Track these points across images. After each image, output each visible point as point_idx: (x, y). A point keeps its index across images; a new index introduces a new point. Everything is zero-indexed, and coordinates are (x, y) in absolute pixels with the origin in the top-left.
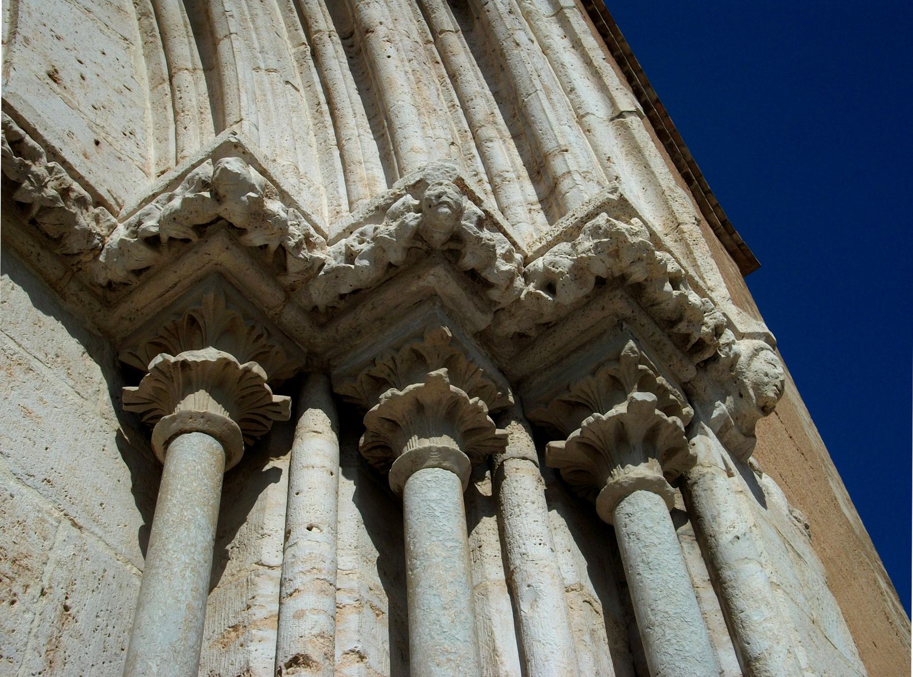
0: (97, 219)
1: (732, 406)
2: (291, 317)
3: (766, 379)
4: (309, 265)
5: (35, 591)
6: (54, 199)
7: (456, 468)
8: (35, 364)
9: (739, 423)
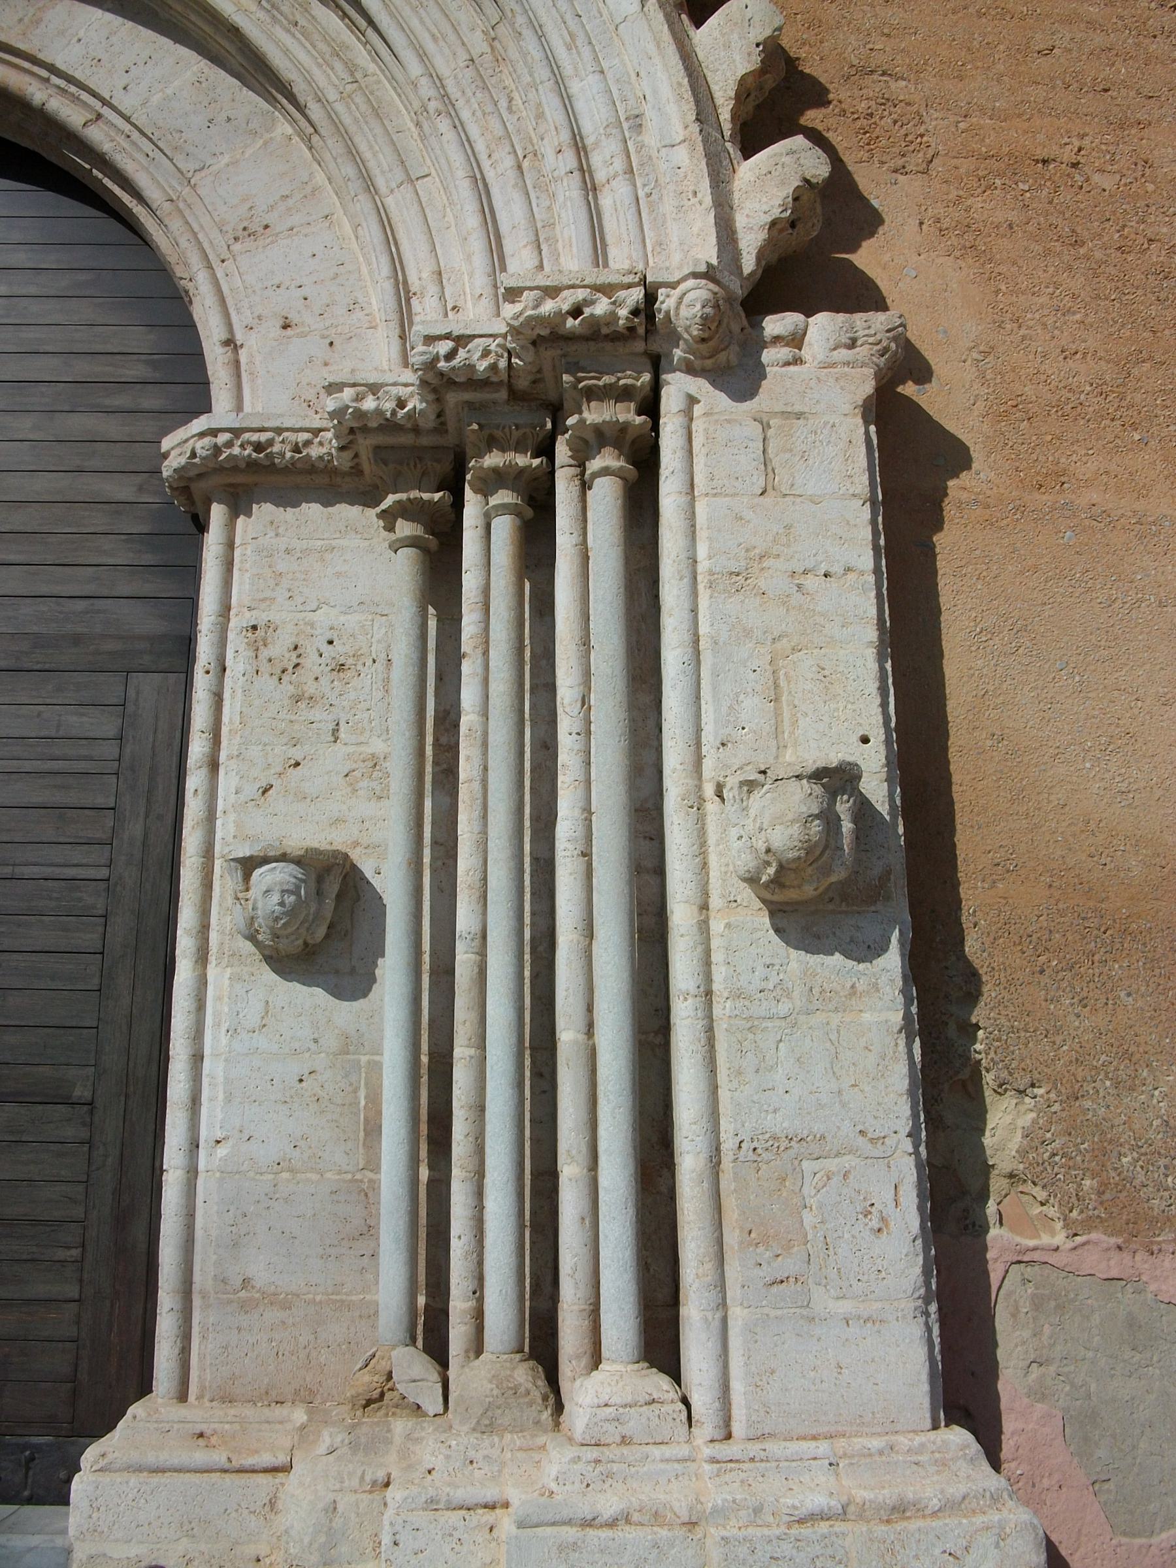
0: (321, 444)
2: (425, 441)
5: (369, 662)
6: (292, 457)
8: (334, 543)
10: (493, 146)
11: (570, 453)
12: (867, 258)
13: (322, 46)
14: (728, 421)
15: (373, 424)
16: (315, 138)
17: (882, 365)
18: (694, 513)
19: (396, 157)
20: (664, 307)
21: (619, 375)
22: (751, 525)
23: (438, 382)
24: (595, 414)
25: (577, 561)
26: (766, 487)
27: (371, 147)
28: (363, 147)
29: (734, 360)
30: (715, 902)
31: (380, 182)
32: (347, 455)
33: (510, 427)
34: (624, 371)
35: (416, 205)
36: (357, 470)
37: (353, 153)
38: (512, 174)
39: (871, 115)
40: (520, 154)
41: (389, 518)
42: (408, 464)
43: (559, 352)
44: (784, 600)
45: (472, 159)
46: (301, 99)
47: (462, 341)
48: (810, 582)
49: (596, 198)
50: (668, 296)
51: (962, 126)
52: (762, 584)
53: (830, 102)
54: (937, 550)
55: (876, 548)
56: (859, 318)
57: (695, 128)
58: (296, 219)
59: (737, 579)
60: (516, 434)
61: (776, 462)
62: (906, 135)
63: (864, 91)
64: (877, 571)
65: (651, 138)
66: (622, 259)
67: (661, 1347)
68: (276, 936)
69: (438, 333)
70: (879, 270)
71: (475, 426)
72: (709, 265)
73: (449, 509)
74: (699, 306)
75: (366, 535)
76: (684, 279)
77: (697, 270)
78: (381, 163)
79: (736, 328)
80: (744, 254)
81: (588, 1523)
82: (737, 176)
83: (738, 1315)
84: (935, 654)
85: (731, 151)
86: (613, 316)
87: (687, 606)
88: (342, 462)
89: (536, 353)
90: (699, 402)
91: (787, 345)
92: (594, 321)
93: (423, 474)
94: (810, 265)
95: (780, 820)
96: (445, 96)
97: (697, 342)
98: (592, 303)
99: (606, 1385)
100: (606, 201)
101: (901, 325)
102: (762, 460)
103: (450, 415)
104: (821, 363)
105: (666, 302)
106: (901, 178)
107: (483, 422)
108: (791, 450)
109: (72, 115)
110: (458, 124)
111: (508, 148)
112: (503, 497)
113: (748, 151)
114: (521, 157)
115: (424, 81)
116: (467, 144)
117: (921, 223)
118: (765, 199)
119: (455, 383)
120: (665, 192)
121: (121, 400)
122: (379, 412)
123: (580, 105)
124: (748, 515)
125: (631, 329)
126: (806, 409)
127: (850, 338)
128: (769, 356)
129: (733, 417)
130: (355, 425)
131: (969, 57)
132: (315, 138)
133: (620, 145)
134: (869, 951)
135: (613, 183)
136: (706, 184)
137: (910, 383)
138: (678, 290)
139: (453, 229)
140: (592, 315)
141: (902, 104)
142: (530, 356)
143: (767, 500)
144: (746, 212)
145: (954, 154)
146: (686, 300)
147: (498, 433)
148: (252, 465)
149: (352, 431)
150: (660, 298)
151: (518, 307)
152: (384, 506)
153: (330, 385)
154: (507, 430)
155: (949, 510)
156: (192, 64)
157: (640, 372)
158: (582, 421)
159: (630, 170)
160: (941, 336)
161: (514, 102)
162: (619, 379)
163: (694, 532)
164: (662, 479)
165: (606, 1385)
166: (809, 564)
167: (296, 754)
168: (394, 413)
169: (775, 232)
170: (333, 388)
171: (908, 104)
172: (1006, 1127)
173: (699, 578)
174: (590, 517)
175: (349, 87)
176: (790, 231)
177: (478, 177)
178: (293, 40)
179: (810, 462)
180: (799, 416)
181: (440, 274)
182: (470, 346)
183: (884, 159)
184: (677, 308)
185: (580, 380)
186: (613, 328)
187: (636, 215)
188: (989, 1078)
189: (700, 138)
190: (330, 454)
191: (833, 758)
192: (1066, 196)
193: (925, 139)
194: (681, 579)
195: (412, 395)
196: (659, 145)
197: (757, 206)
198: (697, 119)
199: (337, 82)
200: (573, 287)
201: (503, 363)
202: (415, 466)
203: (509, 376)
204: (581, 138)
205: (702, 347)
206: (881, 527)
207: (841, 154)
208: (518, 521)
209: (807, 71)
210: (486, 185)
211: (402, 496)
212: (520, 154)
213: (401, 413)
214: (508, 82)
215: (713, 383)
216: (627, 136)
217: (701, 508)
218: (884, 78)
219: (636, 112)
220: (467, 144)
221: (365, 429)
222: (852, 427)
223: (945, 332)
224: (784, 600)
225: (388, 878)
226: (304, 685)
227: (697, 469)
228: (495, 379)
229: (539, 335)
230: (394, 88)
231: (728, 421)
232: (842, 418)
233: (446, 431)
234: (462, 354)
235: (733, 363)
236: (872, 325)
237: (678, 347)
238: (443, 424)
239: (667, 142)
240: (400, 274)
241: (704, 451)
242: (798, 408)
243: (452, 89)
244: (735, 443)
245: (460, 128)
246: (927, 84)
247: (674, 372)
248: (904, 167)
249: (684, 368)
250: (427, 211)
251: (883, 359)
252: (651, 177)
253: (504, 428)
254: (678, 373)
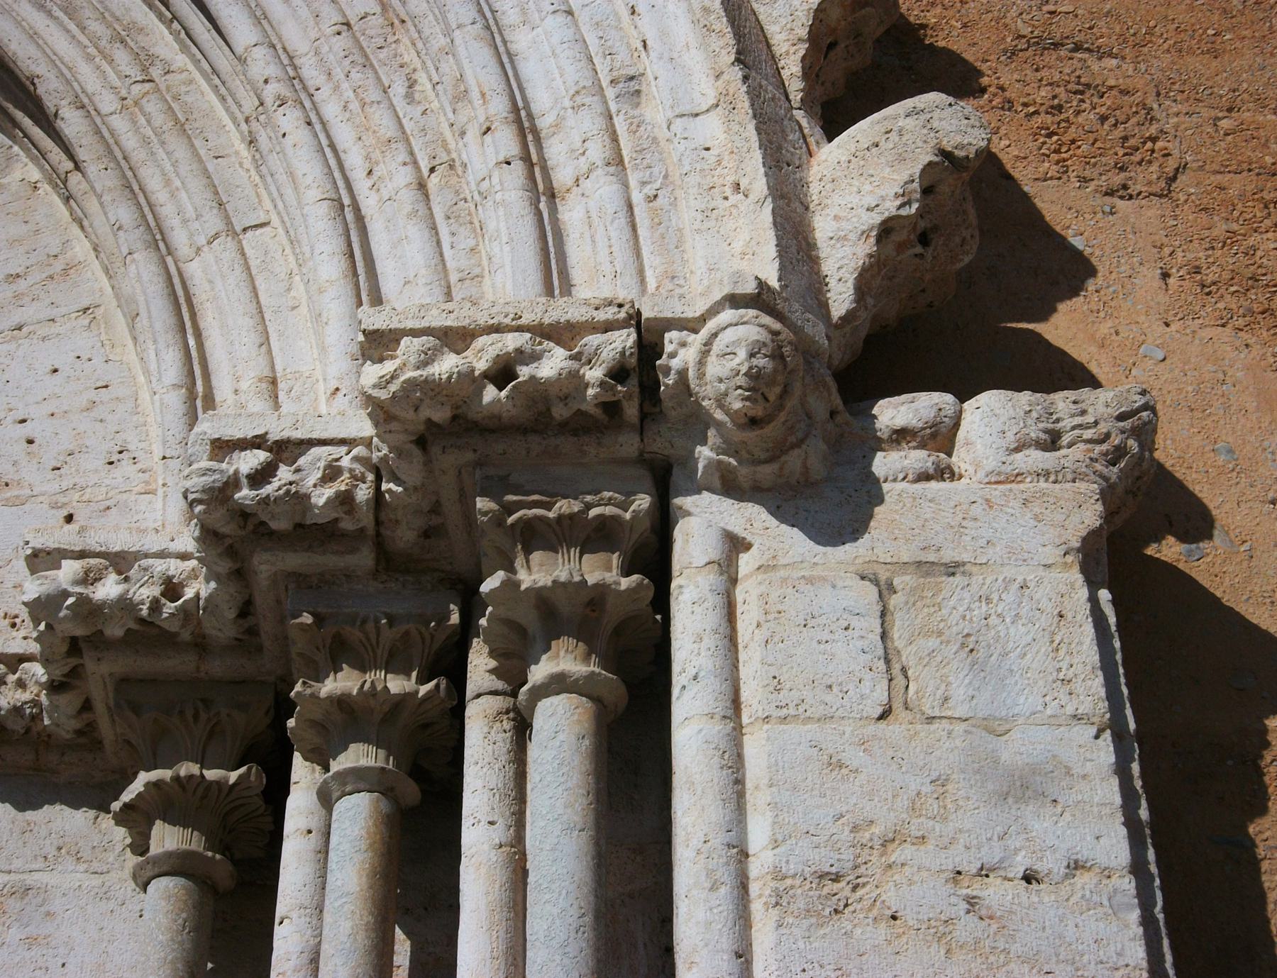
0: (21, 684)
1: (719, 441)
2: (217, 667)
3: (723, 387)
4: (182, 616)
7: (362, 786)
8: (30, 879)
9: (745, 455)
10: (377, 155)
11: (493, 664)
12: (1064, 328)
13: (95, 27)
14: (810, 581)
15: (115, 631)
16: (75, 178)
17: (1114, 478)
18: (740, 756)
19: (209, 195)
20: (675, 363)
21: (589, 498)
22: (862, 777)
23: (235, 528)
25: (502, 875)
27: (168, 182)
28: (153, 183)
29: (817, 468)
31: (180, 239)
32: (69, 702)
33: (377, 621)
34: (597, 492)
35: (239, 270)
36: (87, 737)
37: (133, 189)
38: (408, 197)
39: (1059, 108)
40: (424, 166)
41: (137, 819)
42: (181, 713)
43: (470, 456)
44: (941, 931)
45: (337, 175)
46: (49, 103)
47: (286, 450)
48: (995, 893)
49: (553, 210)
50: (683, 344)
51: (1225, 124)
52: (892, 898)
53: (983, 90)
54: (1261, 852)
55: (1131, 822)
56: (1062, 401)
57: (737, 73)
58: (28, 313)
59: (832, 889)
60: (389, 635)
61: (909, 655)
62: (1125, 138)
63: (1045, 73)
64: (1138, 868)
65: (655, 111)
66: (598, 277)
69: (239, 435)
70: (1093, 349)
71: (307, 619)
72: (761, 284)
73: (260, 802)
74: (742, 354)
75: (96, 866)
76: (713, 311)
77: (740, 290)
79: (819, 408)
80: (832, 283)
82: (814, 161)
85: (804, 123)
86: (574, 381)
87: (726, 943)
88: (58, 718)
89: (428, 463)
90: (748, 547)
91: (922, 446)
92: (539, 393)
93: (211, 735)
94: (965, 300)
96: (295, 78)
97: (741, 427)
98: (535, 357)
100: (572, 214)
101: (1145, 407)
102: (881, 652)
103: (263, 601)
104: (989, 490)
105: (680, 353)
106: (1121, 204)
107: (321, 610)
108: (940, 634)
110: (314, 119)
111: (403, 156)
112: (358, 756)
114: (425, 172)
115: (260, 53)
116: (329, 151)
117: (1165, 276)
118: (867, 187)
119: (272, 533)
120: (680, 193)
122: (125, 605)
123: (530, 69)
124: (854, 757)
125: (611, 408)
126: (965, 557)
127: (1046, 431)
128: (883, 464)
129: (816, 572)
130: (79, 632)
131: (1226, 23)
132: (75, 178)
133: (600, 122)
135: (586, 185)
136: (755, 159)
137: (1171, 540)
138: (704, 333)
139: (304, 309)
140: (532, 378)
141: (1114, 92)
142: (413, 472)
143: (894, 730)
144: (832, 211)
145: (1215, 167)
146: (718, 346)
147: (353, 634)
149: (75, 646)
150: (669, 348)
151: (389, 367)
152: (128, 796)
153: (36, 554)
154: (370, 626)
157: (630, 494)
158: (511, 585)
159: (617, 161)
160: (1222, 458)
161: (417, 88)
162: (589, 507)
163: (741, 795)
164: (675, 691)
166: (992, 854)
168: (155, 606)
169: (890, 249)
170: (41, 560)
171: (1124, 92)
173: (754, 888)
174: (527, 790)
175: (137, 89)
176: (919, 249)
177: (346, 201)
178: (48, 22)
179: (981, 654)
180: (952, 569)
181: (274, 382)
182: (302, 461)
183: (1087, 173)
184: (701, 363)
185: (509, 509)
186: (575, 406)
187: (627, 230)
189: (744, 88)
190: (35, 703)
193: (1160, 144)
194: (713, 888)
195: (194, 575)
196: (670, 114)
197: (854, 200)
198: (738, 60)
199: (117, 83)
200: (497, 329)
201: (363, 493)
202: (196, 717)
203: (378, 522)
204: (530, 116)
205: (751, 435)
206: (1138, 784)
207: (1008, 167)
208: (385, 806)
209: (942, 44)
210: (360, 218)
211: (165, 774)
212: (424, 166)
213: (169, 608)
214: (409, 56)
215: (778, 512)
216: (613, 107)
217: (755, 748)
218: (1079, 55)
219: (631, 72)
220: (329, 151)
221: (98, 641)
222: (1063, 588)
223: (1230, 451)
224: (941, 931)
227: (747, 672)
228: (347, 525)
229: (429, 422)
230: (215, 89)
231: (810, 581)
232: (1041, 572)
233: (260, 649)
234: (284, 473)
237: (704, 442)
238: (253, 632)
239: (686, 108)
240: (199, 383)
241: (760, 635)
242: (948, 555)
243: (311, 72)
244: (823, 620)
245: (318, 127)
246: (1155, 62)
247: (699, 492)
248: (1125, 187)
249: (717, 483)
250: (259, 282)
251: (1115, 470)
252: (656, 170)
253: (364, 622)
254: (706, 494)
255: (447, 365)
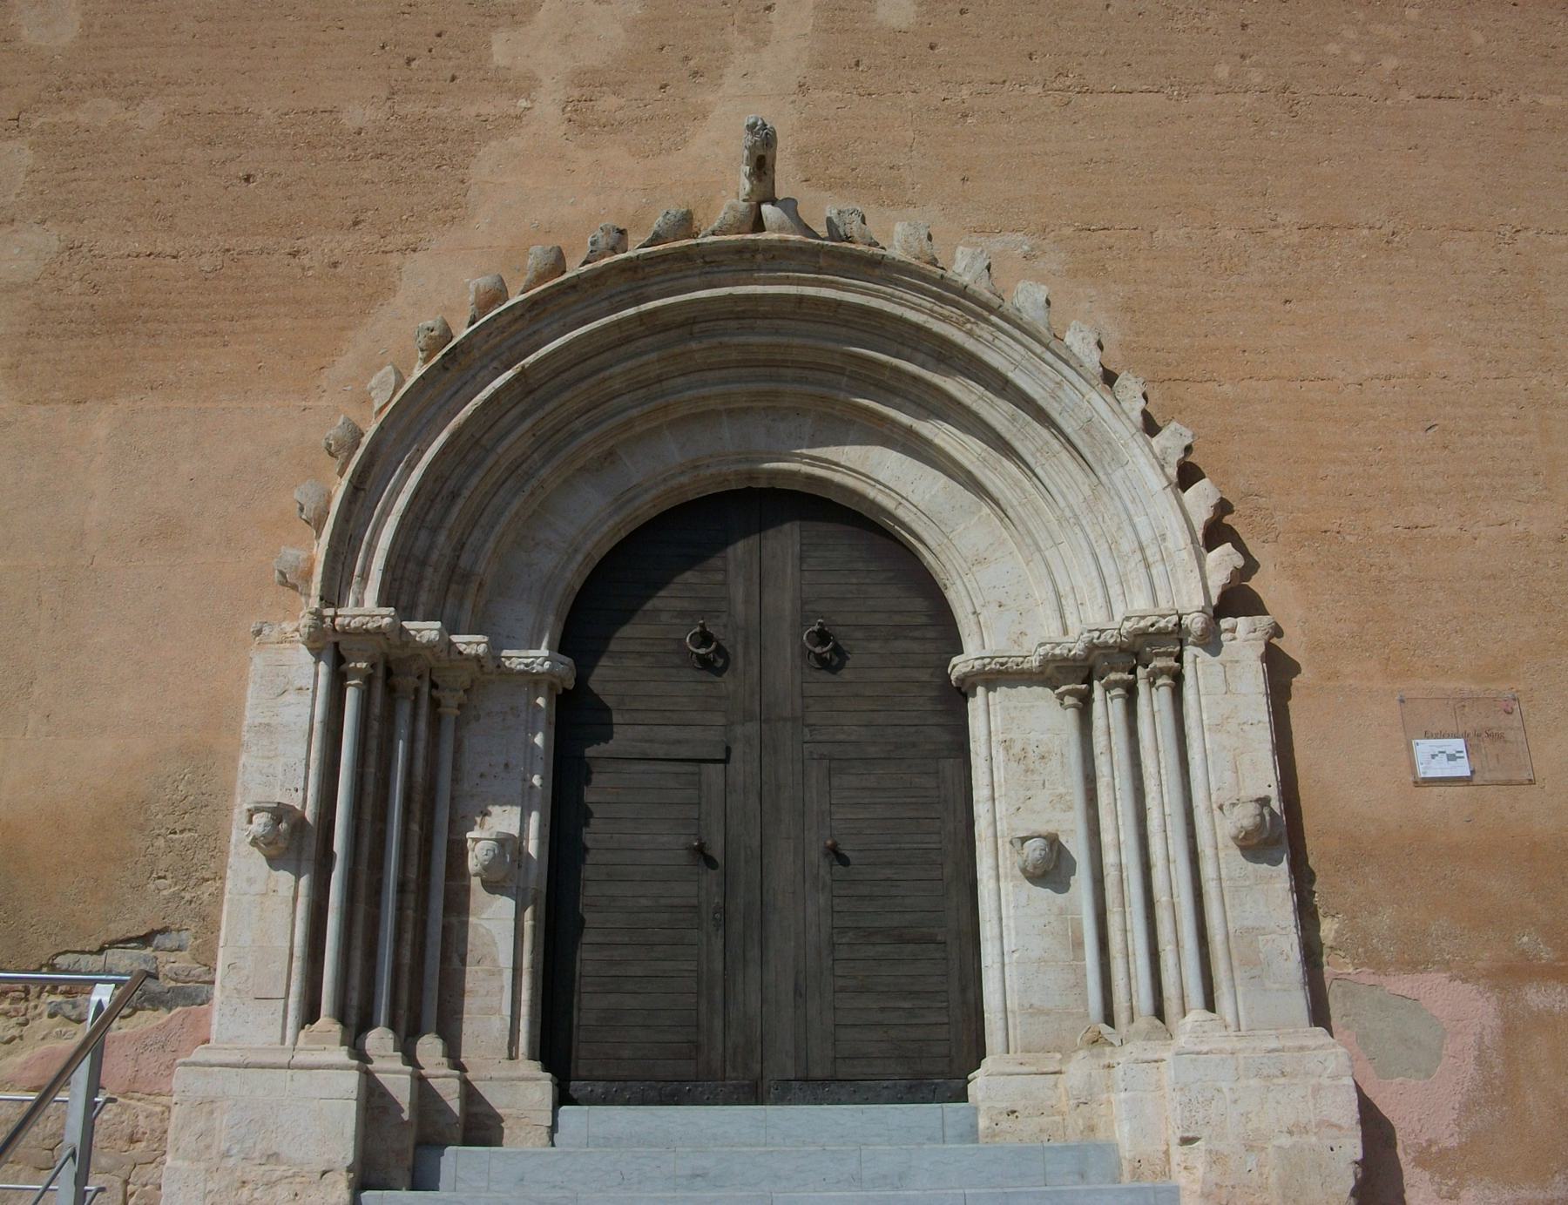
24: (1158, 663)
26: (1226, 686)
30: (1220, 846)
41: (1061, 697)
46: (996, 494)
59: (1218, 727)
64: (463, 961)
65: (1170, 544)
66: (1164, 605)
67: (1210, 1004)
68: (1035, 867)
78: (1041, 537)
81: (1199, 1053)
83: (1240, 990)
84: (1290, 744)
94: (1237, 599)
95: (1245, 817)
96: (1075, 516)
99: (1191, 1022)
100: (1154, 572)
104: (1243, 634)
105: (1186, 621)
109: (889, 504)
113: (1210, 548)
116: (1087, 536)
121: (917, 634)
123: (1139, 528)
128: (1223, 637)
134: (1275, 862)
148: (999, 672)
155: (1293, 691)
156: (943, 479)
165: (1191, 1022)
167: (1029, 794)
172: (1328, 929)
188: (1321, 911)
191: (1262, 794)
192: (1335, 548)
220: (1087, 536)
225: (1077, 847)
226: (1019, 765)
235: (1211, 641)
236: (1263, 622)
255: (1142, 624)
